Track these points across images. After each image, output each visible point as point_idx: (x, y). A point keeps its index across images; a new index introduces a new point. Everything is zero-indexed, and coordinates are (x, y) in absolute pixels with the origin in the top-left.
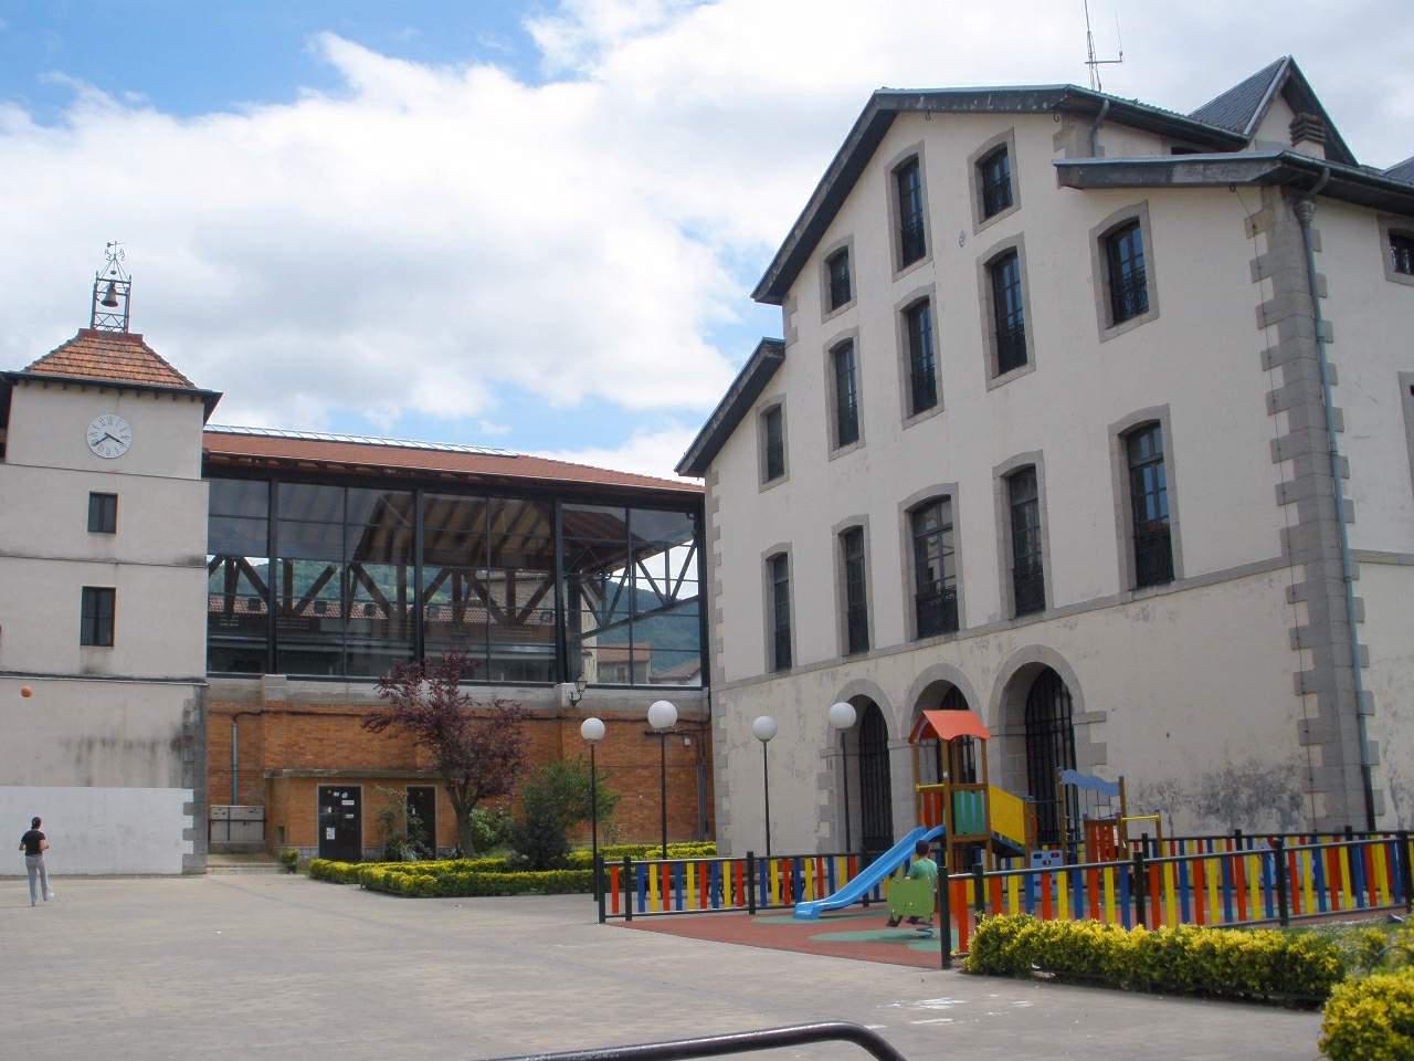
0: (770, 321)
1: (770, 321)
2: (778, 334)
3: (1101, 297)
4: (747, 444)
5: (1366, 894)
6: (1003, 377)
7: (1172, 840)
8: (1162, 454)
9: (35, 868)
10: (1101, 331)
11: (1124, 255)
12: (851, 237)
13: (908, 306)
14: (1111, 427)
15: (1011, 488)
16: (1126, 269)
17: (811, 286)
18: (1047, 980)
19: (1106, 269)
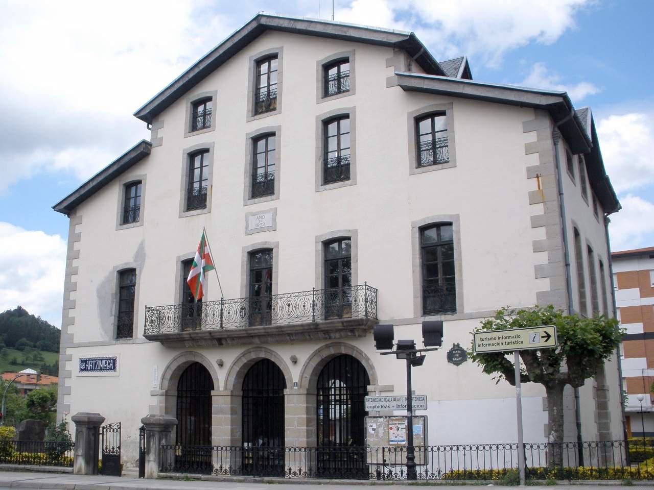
0: (142, 132)
1: (142, 132)
2: (148, 139)
3: (120, 211)
4: (112, 200)
5: (207, 461)
6: (252, 201)
7: (35, 442)
8: (135, 283)
9: (256, 291)
10: (317, 186)
11: (133, 194)
12: (216, 91)
13: (325, 119)
14: (178, 257)
15: (251, 258)
16: (196, 185)
17: (180, 115)
18: (619, 485)
19: (80, 206)
